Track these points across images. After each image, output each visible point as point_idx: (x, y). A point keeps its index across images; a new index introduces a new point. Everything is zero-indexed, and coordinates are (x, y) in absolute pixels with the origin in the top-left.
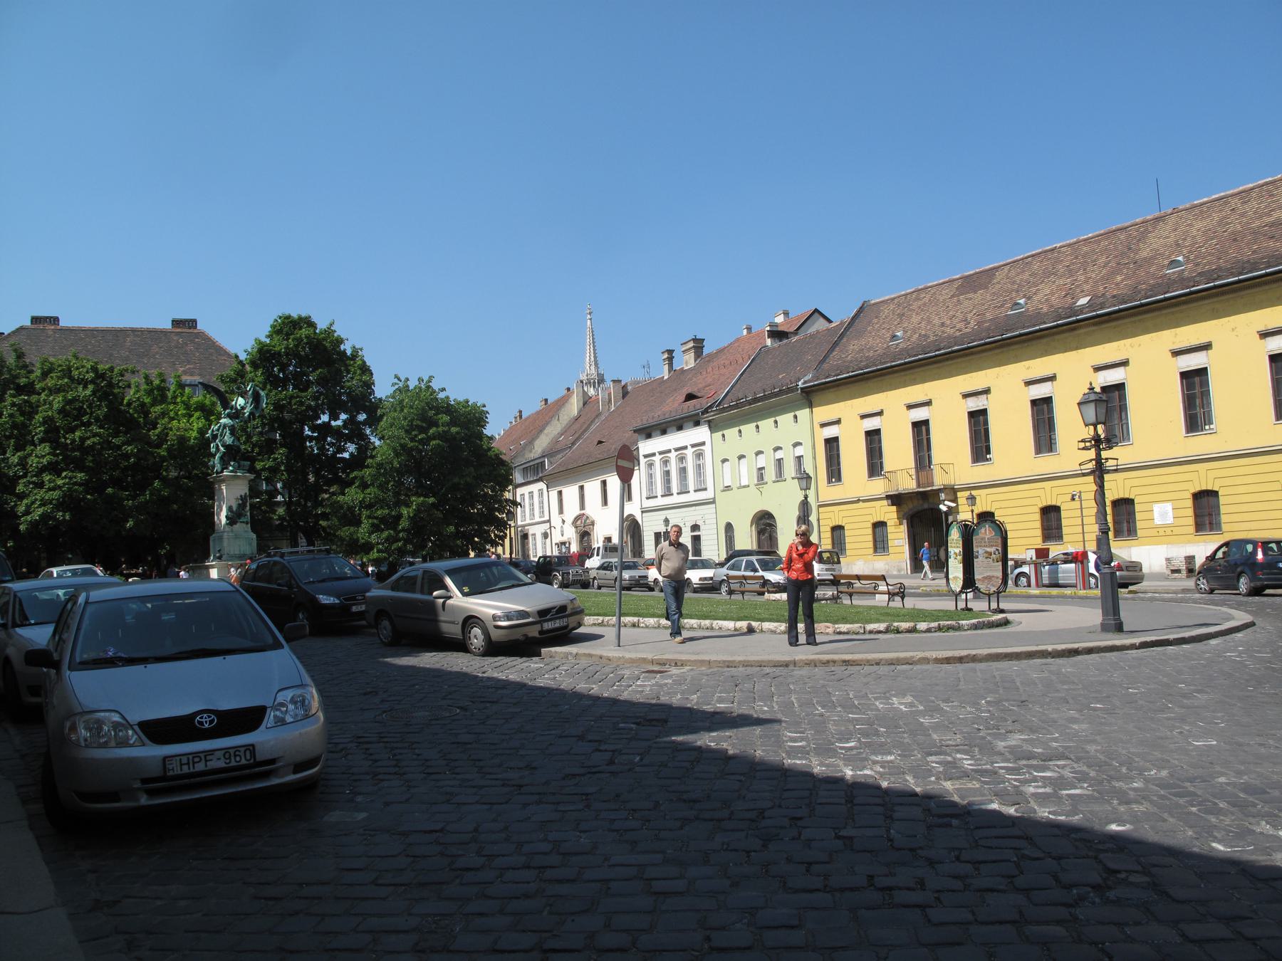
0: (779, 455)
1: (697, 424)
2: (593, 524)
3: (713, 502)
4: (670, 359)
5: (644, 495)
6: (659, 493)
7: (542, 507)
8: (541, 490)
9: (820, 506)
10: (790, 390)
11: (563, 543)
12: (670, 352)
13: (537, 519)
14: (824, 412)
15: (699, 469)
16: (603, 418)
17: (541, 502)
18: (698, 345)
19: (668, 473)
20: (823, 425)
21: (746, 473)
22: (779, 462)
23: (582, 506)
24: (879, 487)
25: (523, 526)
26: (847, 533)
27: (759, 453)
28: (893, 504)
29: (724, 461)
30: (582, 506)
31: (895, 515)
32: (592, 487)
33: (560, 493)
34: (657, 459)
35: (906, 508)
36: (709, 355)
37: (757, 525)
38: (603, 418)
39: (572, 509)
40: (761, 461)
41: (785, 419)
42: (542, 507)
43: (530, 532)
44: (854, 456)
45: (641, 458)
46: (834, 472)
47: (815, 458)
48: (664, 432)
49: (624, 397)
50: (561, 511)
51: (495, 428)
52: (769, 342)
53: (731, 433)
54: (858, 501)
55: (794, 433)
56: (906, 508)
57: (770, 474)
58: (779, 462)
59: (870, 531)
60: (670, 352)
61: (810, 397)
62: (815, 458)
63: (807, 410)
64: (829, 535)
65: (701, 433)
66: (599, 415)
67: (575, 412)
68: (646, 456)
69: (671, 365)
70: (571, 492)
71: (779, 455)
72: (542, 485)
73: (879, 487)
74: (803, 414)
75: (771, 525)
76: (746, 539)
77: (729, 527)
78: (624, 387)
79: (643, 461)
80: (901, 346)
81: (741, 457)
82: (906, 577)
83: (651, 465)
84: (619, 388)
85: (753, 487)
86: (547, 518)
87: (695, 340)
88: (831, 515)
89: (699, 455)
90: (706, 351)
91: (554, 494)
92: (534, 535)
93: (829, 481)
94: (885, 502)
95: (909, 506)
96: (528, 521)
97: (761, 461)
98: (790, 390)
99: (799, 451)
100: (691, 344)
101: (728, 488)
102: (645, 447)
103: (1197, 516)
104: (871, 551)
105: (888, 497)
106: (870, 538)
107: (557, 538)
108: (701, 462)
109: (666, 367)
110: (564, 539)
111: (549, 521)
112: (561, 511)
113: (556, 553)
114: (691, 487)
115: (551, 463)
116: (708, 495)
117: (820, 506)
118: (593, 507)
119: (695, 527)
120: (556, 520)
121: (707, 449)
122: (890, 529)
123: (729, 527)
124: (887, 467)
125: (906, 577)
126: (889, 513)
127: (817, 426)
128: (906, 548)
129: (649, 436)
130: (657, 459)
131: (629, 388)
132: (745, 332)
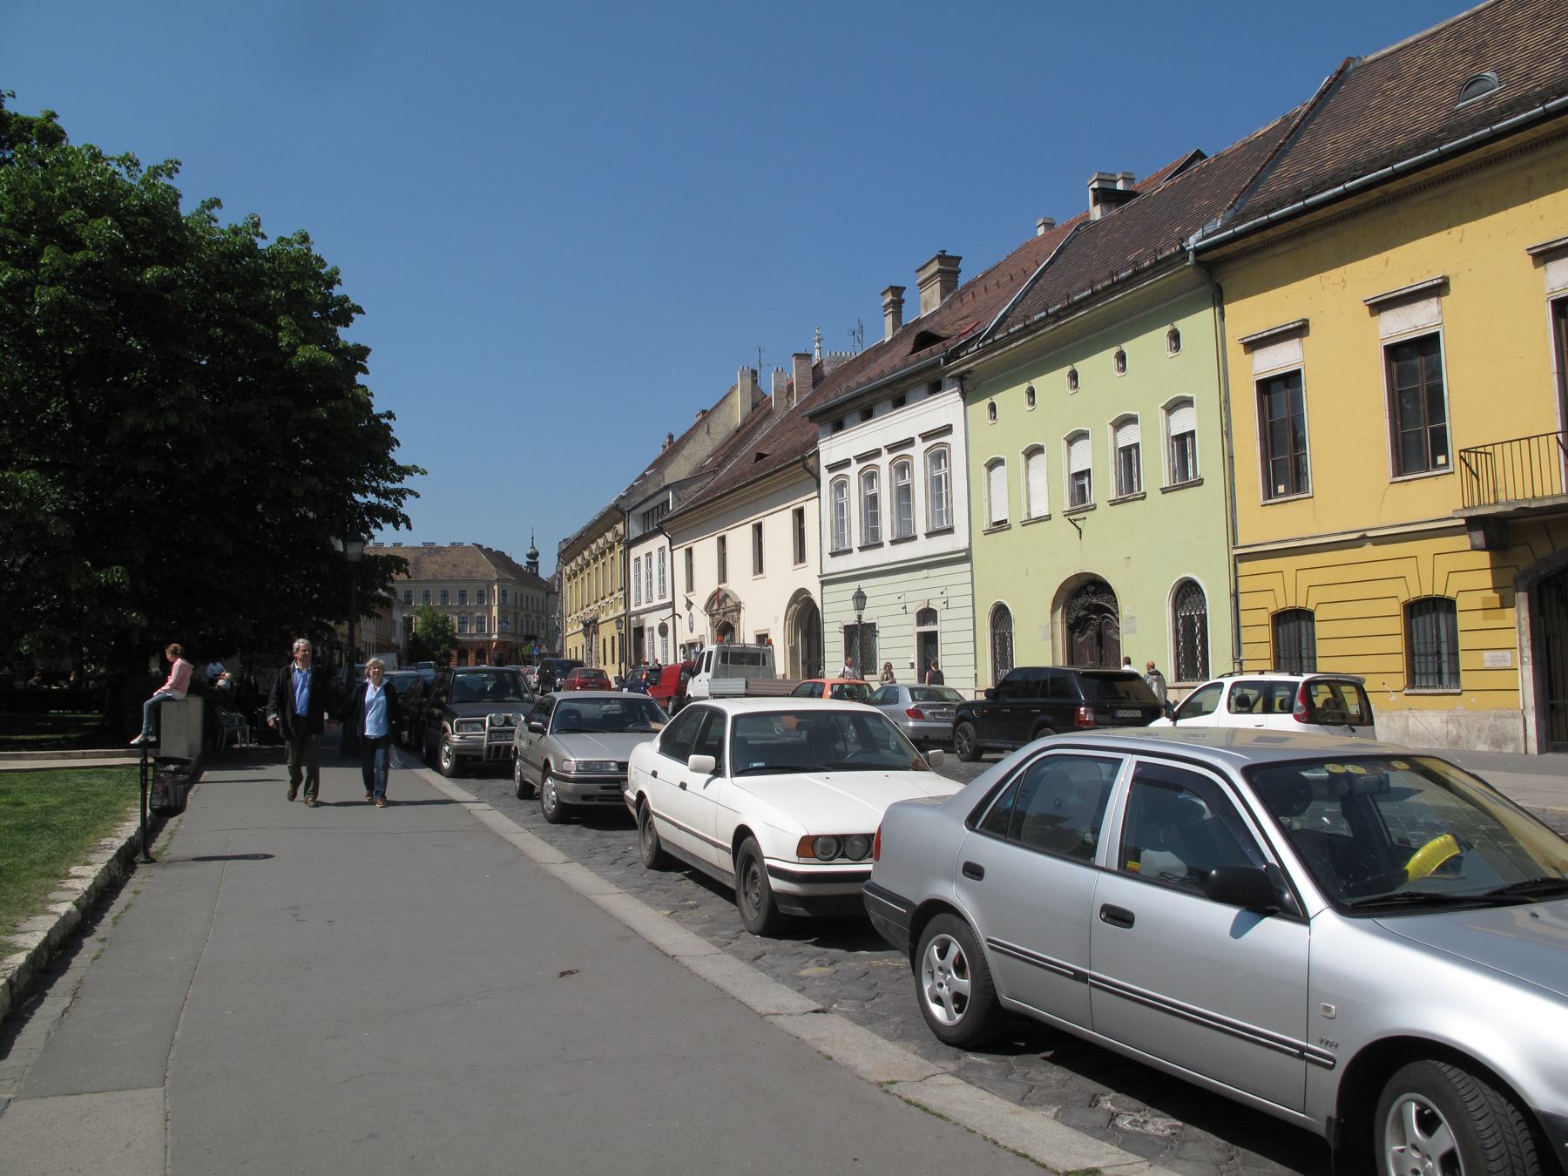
0: (1128, 436)
1: (936, 388)
2: (738, 608)
3: (965, 557)
4: (897, 304)
5: (827, 549)
6: (856, 542)
7: (662, 580)
8: (662, 549)
9: (1240, 558)
10: (1168, 263)
11: (692, 645)
12: (897, 291)
13: (657, 602)
14: (1252, 312)
15: (938, 486)
16: (776, 420)
17: (662, 571)
18: (949, 268)
19: (873, 501)
20: (1253, 345)
21: (1044, 488)
22: (1129, 455)
23: (723, 577)
24: (1438, 496)
25: (638, 614)
26: (1320, 630)
27: (1077, 436)
28: (1487, 547)
29: (994, 464)
30: (723, 577)
31: (1486, 579)
32: (739, 538)
33: (689, 552)
34: (853, 471)
35: (1525, 559)
36: (968, 286)
37: (1068, 609)
38: (776, 420)
39: (706, 583)
40: (1082, 457)
41: (1148, 346)
42: (662, 580)
43: (647, 625)
44: (1348, 416)
45: (824, 473)
46: (1285, 463)
47: (1227, 433)
48: (868, 415)
49: (814, 385)
50: (690, 587)
51: (187, 208)
52: (1096, 213)
53: (1011, 399)
54: (1361, 541)
55: (1177, 373)
56: (1525, 559)
57: (1104, 485)
58: (1129, 455)
59: (1397, 625)
60: (897, 291)
61: (1214, 277)
62: (1227, 433)
63: (1208, 315)
64: (1266, 634)
65: (945, 408)
66: (770, 413)
67: (738, 420)
68: (831, 468)
69: (897, 315)
70: (705, 549)
71: (1128, 436)
72: (662, 541)
73: (1438, 496)
74: (1198, 325)
75: (1100, 610)
76: (1039, 646)
77: (1001, 615)
78: (817, 368)
79: (826, 477)
80: (1502, 97)
81: (1033, 451)
82: (1518, 764)
83: (840, 486)
84: (807, 369)
85: (1060, 521)
86: (669, 599)
87: (942, 257)
88: (1273, 581)
89: (938, 457)
90: (963, 280)
91: (680, 555)
92: (651, 629)
93: (1270, 492)
94: (1463, 541)
95: (1536, 553)
96: (644, 606)
97: (1082, 457)
98: (1168, 263)
99: (1183, 421)
100: (935, 267)
101: (1001, 526)
102: (832, 449)
103: (1411, 654)
104: (1401, 681)
105: (1473, 523)
106: (1398, 644)
107: (684, 637)
108: (943, 470)
109: (889, 320)
110: (694, 637)
111: (672, 605)
112: (690, 587)
113: (681, 660)
114: (921, 528)
115: (678, 499)
116: (957, 541)
117: (1240, 558)
118: (740, 582)
119: (927, 615)
120: (680, 607)
121: (955, 441)
122: (1463, 621)
123: (1001, 615)
124: (1458, 438)
125: (1518, 764)
126: (1465, 573)
127: (1235, 349)
128: (1526, 678)
129: (839, 426)
130: (853, 471)
131: (827, 370)
132: (1041, 231)
